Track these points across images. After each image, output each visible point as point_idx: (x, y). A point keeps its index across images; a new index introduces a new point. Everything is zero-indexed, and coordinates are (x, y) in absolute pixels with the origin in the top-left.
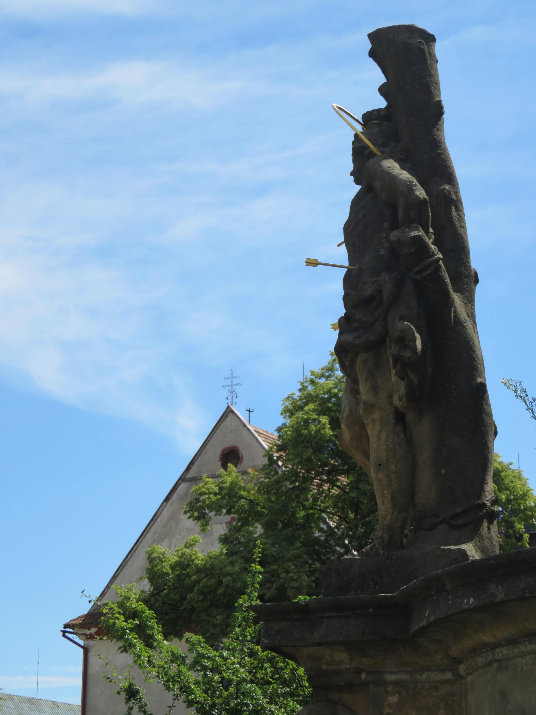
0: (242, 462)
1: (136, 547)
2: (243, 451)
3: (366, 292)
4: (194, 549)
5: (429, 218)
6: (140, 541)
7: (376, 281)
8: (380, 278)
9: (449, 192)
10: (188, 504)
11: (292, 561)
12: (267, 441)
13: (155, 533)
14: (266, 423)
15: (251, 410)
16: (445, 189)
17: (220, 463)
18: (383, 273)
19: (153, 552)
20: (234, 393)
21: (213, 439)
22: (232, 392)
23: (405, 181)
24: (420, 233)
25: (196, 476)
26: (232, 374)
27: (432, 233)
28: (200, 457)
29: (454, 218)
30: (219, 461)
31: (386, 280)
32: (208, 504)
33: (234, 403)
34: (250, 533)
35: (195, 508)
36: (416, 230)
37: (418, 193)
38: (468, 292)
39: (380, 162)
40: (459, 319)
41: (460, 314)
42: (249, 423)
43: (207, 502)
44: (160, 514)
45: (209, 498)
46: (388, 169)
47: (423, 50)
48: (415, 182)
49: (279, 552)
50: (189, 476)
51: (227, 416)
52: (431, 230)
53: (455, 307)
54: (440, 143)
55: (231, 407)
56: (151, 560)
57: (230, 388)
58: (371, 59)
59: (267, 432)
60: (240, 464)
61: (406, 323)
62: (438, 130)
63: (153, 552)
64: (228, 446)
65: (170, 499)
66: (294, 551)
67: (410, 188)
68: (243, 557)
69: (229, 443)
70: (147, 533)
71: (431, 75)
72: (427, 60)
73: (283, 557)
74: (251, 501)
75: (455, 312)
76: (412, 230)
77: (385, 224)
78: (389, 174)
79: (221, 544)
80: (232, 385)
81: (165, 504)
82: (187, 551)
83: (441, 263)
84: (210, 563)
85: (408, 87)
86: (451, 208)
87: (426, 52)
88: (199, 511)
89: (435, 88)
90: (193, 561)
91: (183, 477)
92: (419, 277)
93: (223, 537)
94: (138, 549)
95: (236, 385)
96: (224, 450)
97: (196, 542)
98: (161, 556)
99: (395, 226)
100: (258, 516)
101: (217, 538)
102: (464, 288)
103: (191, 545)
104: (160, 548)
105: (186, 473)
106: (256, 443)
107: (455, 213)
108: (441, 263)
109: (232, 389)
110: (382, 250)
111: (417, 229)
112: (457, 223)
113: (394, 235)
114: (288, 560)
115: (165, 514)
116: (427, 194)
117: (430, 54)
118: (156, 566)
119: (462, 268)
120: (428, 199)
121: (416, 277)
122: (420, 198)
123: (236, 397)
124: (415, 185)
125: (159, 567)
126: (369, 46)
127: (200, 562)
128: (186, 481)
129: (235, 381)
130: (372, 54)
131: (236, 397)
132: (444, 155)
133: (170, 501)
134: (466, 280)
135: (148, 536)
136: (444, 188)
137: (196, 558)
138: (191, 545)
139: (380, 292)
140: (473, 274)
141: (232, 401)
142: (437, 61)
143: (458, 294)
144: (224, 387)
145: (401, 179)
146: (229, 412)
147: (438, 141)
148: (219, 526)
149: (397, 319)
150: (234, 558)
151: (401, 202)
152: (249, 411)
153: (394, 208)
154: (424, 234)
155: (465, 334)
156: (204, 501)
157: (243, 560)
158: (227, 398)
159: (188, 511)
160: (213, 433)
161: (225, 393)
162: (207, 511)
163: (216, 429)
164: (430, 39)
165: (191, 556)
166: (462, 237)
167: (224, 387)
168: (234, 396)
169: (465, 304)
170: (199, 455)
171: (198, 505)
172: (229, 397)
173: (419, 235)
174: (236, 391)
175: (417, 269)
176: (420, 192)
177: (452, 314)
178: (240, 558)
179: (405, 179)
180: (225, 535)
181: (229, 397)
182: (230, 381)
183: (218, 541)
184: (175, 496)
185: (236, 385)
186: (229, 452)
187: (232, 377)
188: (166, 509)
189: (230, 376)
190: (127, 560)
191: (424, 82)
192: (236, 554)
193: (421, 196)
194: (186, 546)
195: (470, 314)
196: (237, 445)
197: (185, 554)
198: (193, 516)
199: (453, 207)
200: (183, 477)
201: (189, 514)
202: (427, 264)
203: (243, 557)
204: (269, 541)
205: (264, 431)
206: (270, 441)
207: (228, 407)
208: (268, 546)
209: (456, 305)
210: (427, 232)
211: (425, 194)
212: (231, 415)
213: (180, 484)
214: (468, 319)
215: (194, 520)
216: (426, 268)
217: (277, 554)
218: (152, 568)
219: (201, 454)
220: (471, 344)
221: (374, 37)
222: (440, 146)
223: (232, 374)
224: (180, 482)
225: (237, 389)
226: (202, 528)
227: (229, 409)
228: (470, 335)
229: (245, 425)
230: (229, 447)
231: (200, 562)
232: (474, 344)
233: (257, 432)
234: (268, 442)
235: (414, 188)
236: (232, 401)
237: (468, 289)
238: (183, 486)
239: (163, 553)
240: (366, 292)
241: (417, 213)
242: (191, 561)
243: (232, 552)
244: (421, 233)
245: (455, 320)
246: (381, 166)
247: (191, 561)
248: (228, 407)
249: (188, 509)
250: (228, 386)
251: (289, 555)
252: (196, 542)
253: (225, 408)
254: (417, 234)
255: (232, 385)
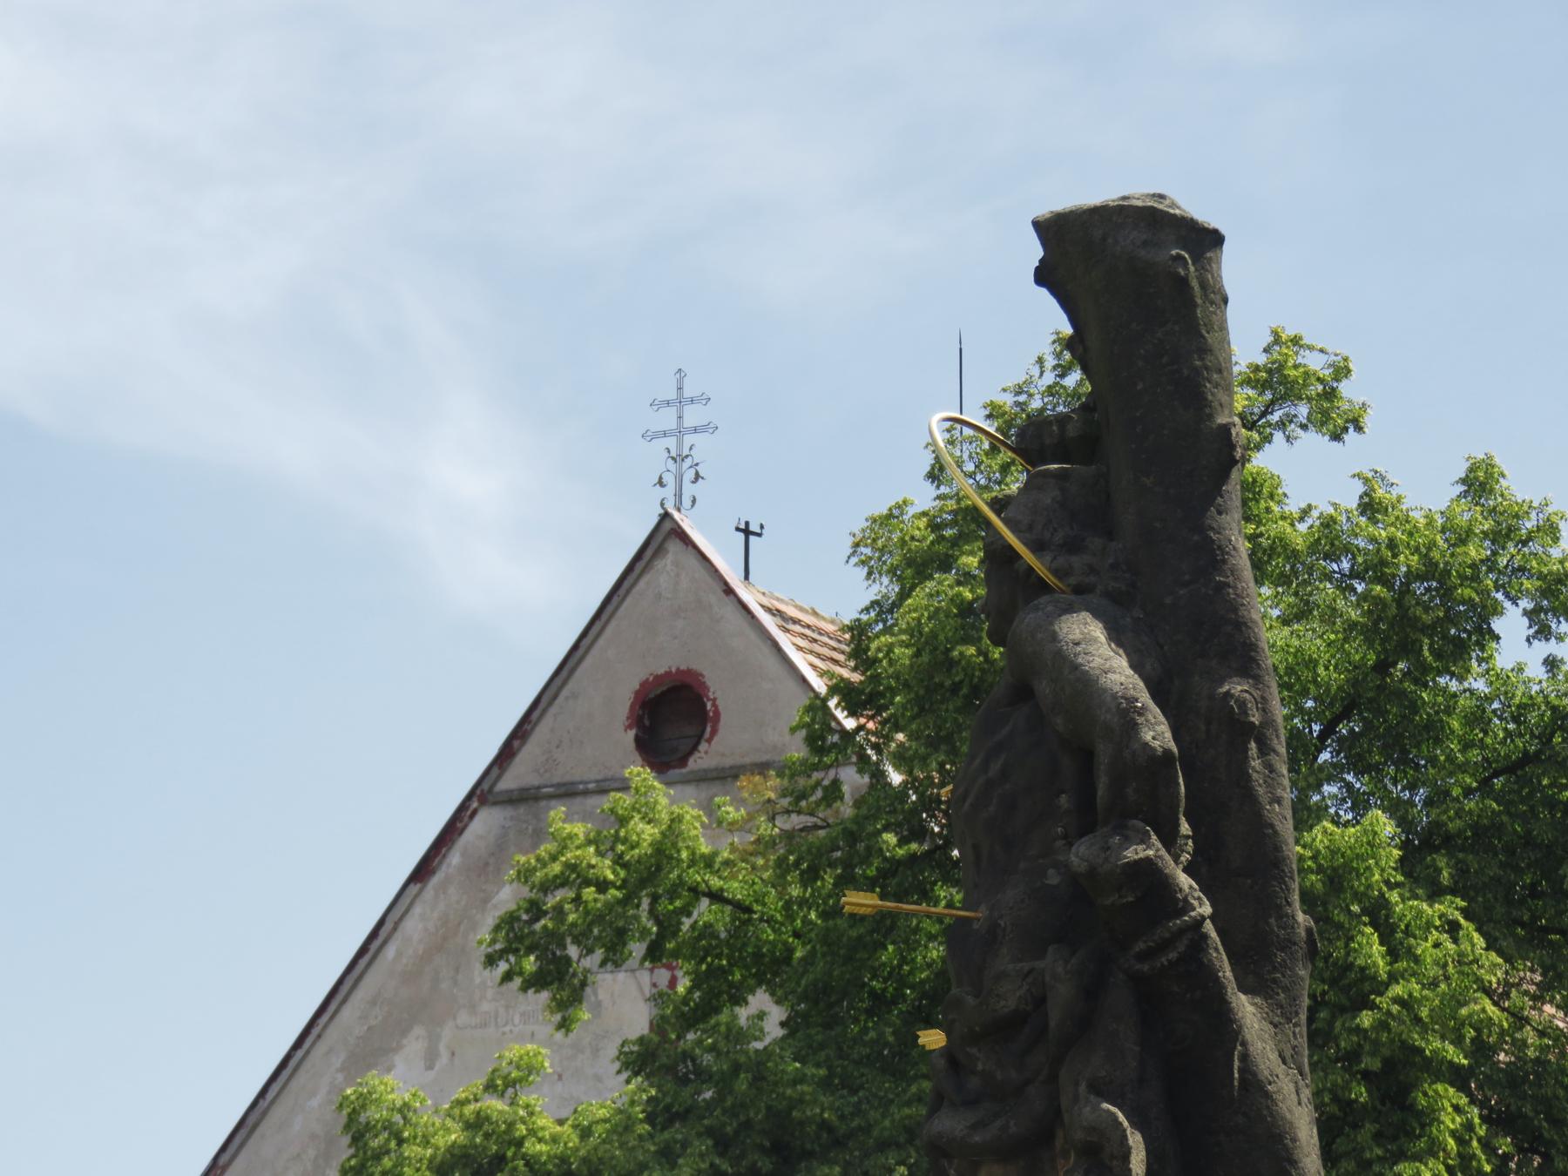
0: (714, 732)
1: (300, 1053)
2: (721, 691)
3: (1003, 1003)
4: (523, 1099)
5: (1179, 801)
6: (315, 1031)
7: (1030, 972)
8: (1040, 964)
9: (1242, 704)
10: (497, 928)
11: (898, 1146)
12: (816, 648)
13: (373, 1002)
14: (809, 587)
15: (754, 527)
16: (1232, 696)
17: (632, 733)
18: (1050, 949)
19: (364, 1101)
20: (688, 462)
21: (601, 642)
22: (678, 459)
23: (1114, 696)
24: (1151, 853)
25: (536, 783)
26: (680, 388)
27: (1188, 837)
28: (553, 710)
29: (1255, 776)
30: (629, 727)
31: (1059, 971)
32: (574, 925)
33: (686, 502)
34: (737, 1036)
35: (527, 942)
36: (1142, 842)
37: (1148, 736)
38: (1286, 989)
39: (1052, 624)
40: (1255, 1075)
41: (1259, 1060)
42: (747, 577)
43: (571, 918)
44: (395, 929)
45: (577, 900)
46: (1070, 650)
47: (1184, 282)
48: (1145, 698)
49: (847, 1110)
50: (509, 782)
51: (660, 551)
52: (1185, 828)
53: (1244, 1044)
54: (1224, 553)
55: (676, 515)
56: (358, 1133)
57: (671, 442)
58: (1044, 292)
59: (815, 613)
60: (709, 741)
61: (1105, 1106)
62: (1220, 513)
63: (364, 1101)
64: (661, 671)
65: (433, 872)
66: (907, 1111)
67: (1128, 716)
68: (710, 1132)
69: (665, 662)
70: (344, 1001)
71: (1204, 350)
72: (1195, 305)
73: (867, 1129)
74: (740, 907)
75: (1245, 1057)
76: (1127, 841)
77: (1063, 799)
78: (1076, 667)
79: (625, 1075)
80: (680, 432)
81: (414, 889)
82: (495, 1105)
83: (1208, 926)
84: (582, 1153)
85: (1140, 386)
86: (1246, 750)
87: (1195, 284)
88: (542, 954)
89: (1217, 386)
90: (519, 1143)
91: (485, 786)
92: (1146, 968)
93: (636, 1048)
94: (307, 1065)
95: (695, 430)
96: (644, 684)
97: (531, 1070)
98: (397, 1118)
99: (1087, 821)
100: (769, 969)
101: (614, 1052)
102: (1275, 981)
103: (510, 1083)
104: (395, 1084)
105: (495, 771)
106: (772, 662)
107: (1256, 763)
108: (1208, 926)
109: (680, 444)
110: (1051, 872)
111: (1144, 840)
112: (1261, 791)
113: (1081, 854)
114: (883, 1146)
115: (415, 927)
116: (1175, 739)
117: (1204, 286)
118: (377, 1157)
119: (1272, 921)
120: (1175, 750)
121: (1138, 966)
122: (1153, 749)
123: (697, 477)
124: (1142, 712)
125: (387, 1162)
126: (1036, 252)
127: (544, 1148)
128: (495, 803)
129: (693, 416)
130: (1043, 276)
131: (697, 477)
132: (1235, 588)
133: (435, 880)
134: (1280, 956)
135: (349, 1014)
136: (1228, 693)
137: (532, 1132)
138: (510, 1083)
139: (1041, 1002)
140: (1303, 934)
141: (679, 495)
142: (1225, 301)
143: (1258, 1000)
144: (650, 436)
145: (1105, 690)
146: (666, 535)
147: (1220, 547)
148: (625, 1001)
149: (1083, 1088)
150: (677, 1132)
151: (1104, 754)
152: (747, 532)
153: (1087, 757)
154: (1163, 852)
155: (1272, 1115)
156: (559, 911)
157: (710, 1142)
158: (661, 483)
159: (502, 954)
160: (604, 617)
161: (655, 458)
162: (573, 951)
163: (615, 600)
164: (1206, 240)
165: (511, 1125)
166: (1276, 832)
167: (650, 436)
168: (690, 475)
169: (1275, 1026)
170: (550, 703)
171: (538, 926)
172: (669, 479)
173: (1148, 859)
174: (697, 456)
175: (1140, 946)
176: (1157, 732)
177: (1236, 1063)
178: (699, 1135)
179: (1117, 688)
180: (641, 1040)
181: (669, 479)
182: (671, 412)
183: (617, 1065)
184: (455, 858)
185: (695, 430)
186: (663, 694)
187: (681, 401)
188: (417, 910)
189: (672, 394)
190: (263, 1104)
191: (1186, 372)
192: (684, 1115)
193: (1156, 744)
194: (490, 1087)
195: (1288, 1053)
196: (696, 666)
197: (488, 1118)
198: (521, 973)
199: (1253, 745)
200: (485, 786)
201: (503, 966)
202: (1167, 935)
203: (710, 1132)
204: (810, 1071)
205: (801, 609)
206: (825, 651)
207: (666, 516)
208: (805, 1088)
209: (1248, 1037)
210: (1170, 839)
211: (1168, 735)
212: (674, 547)
213: (475, 812)
214: (1281, 1069)
215: (524, 988)
216: (1165, 946)
217: (842, 1117)
218: (363, 1166)
219: (555, 697)
220: (1288, 1141)
221: (1052, 230)
222: (1224, 561)
223: (680, 388)
224: (475, 805)
225: (701, 446)
226: (558, 1017)
227: (667, 525)
228: (1283, 1118)
229: (729, 591)
230: (668, 674)
231: (544, 1148)
232: (1294, 1140)
233: (768, 610)
234: (818, 656)
235: (1140, 720)
236: (679, 495)
237: (1286, 981)
238: (485, 823)
239: (404, 1109)
240: (1003, 1003)
241: (1143, 793)
242: (510, 1143)
243: (668, 1108)
244: (1150, 849)
245: (1242, 1080)
246: (1054, 637)
247: (510, 1143)
248: (666, 516)
249: (498, 946)
250: (665, 434)
251: (887, 1123)
252: (531, 1070)
253: (655, 520)
254: (1141, 855)
255: (680, 432)
